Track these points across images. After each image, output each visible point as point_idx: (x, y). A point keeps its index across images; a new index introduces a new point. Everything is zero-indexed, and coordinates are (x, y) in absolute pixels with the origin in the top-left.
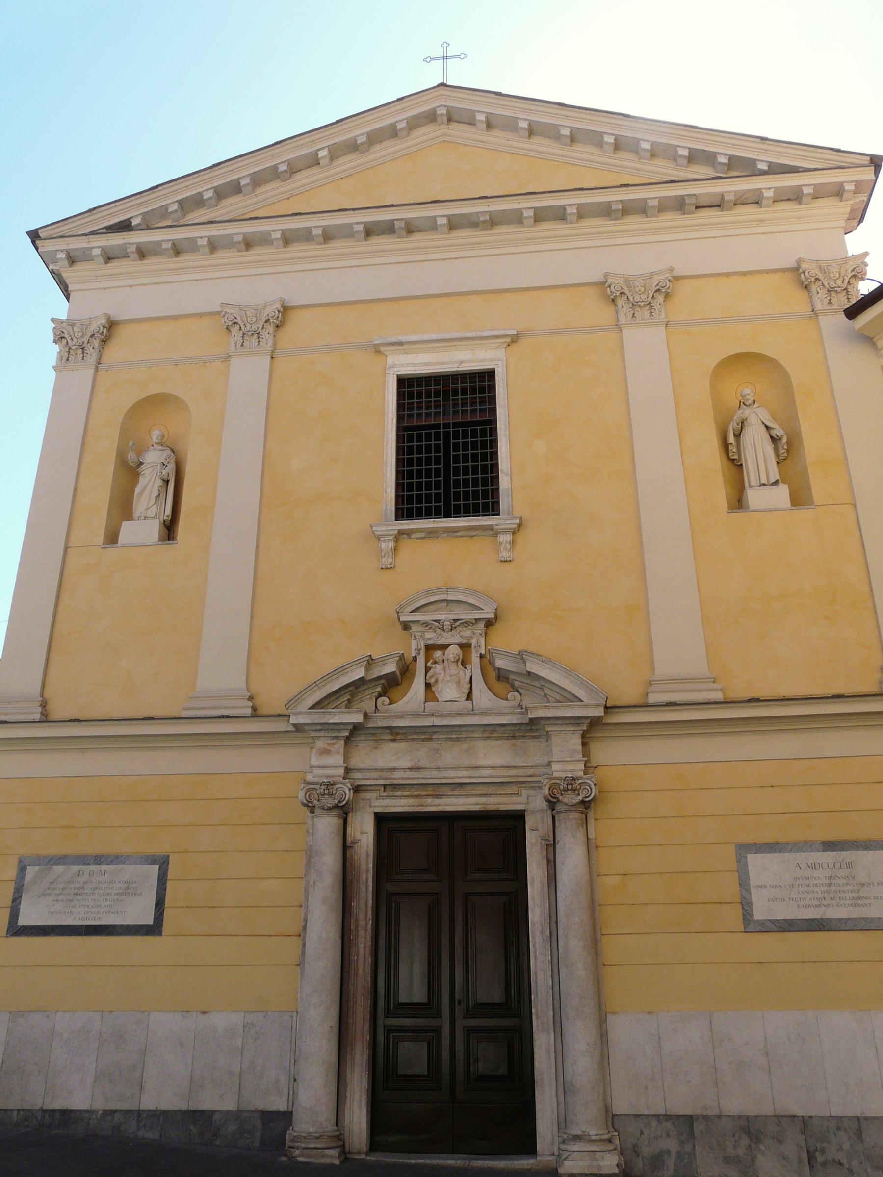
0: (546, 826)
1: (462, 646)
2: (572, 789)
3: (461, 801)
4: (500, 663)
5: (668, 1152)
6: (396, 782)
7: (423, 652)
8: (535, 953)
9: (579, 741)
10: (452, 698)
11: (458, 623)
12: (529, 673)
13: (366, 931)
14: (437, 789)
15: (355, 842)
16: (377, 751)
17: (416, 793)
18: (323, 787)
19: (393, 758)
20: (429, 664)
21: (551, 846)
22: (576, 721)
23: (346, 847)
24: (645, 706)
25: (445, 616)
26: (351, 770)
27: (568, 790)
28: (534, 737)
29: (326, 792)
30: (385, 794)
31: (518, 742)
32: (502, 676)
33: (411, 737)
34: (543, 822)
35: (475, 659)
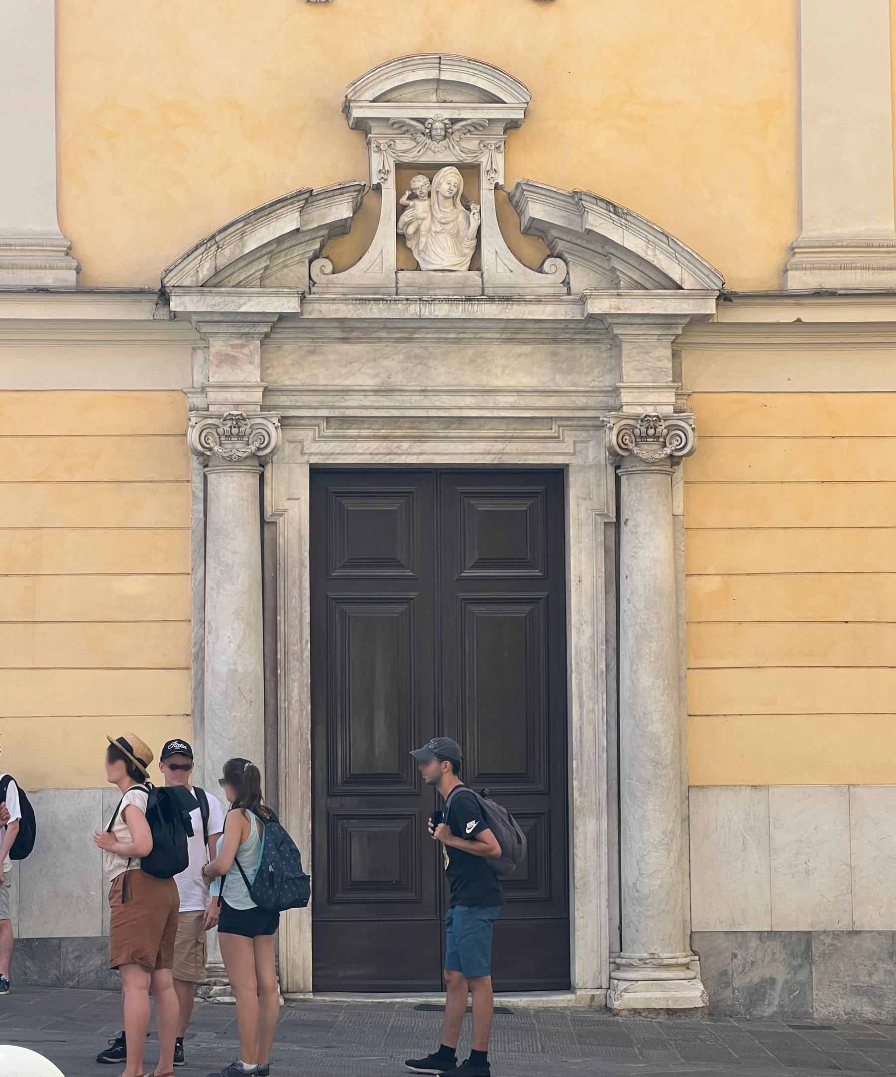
0: (603, 493)
1: (461, 167)
2: (654, 436)
3: (461, 447)
4: (536, 210)
5: (773, 981)
6: (349, 413)
7: (392, 178)
8: (580, 697)
9: (669, 353)
10: (446, 265)
11: (457, 126)
12: (589, 231)
13: (301, 661)
14: (419, 426)
15: (281, 513)
16: (312, 358)
17: (383, 432)
18: (229, 423)
19: (353, 374)
20: (404, 200)
21: (615, 527)
22: (666, 321)
23: (266, 524)
24: (780, 296)
25: (437, 113)
26: (270, 390)
27: (648, 436)
28: (588, 341)
29: (235, 431)
30: (328, 433)
31: (562, 348)
32: (537, 231)
33: (373, 335)
34: (599, 486)
35: (487, 196)
